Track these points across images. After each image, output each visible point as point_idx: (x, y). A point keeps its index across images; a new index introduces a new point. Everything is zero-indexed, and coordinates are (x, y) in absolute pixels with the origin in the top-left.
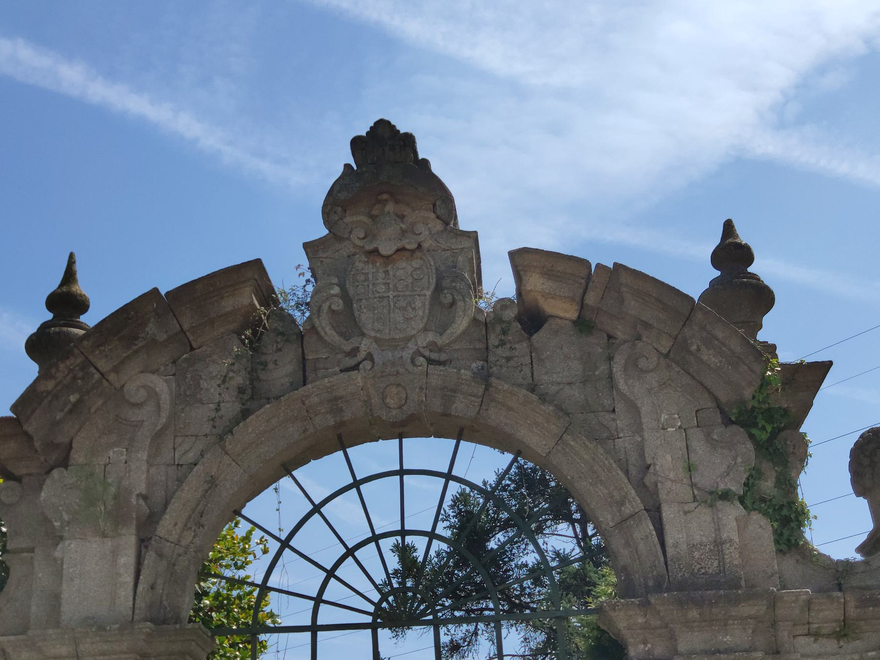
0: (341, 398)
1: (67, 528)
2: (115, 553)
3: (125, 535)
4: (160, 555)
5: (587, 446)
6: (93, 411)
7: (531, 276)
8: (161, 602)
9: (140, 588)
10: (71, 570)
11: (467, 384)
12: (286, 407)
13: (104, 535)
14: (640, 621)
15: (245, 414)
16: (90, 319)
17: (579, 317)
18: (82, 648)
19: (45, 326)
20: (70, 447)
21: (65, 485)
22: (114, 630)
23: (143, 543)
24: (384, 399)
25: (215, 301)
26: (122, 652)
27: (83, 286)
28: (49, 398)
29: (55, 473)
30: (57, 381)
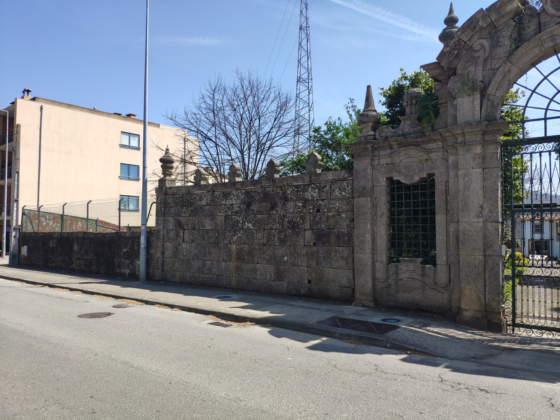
0: (556, 35)
4: (489, 100)
9: (482, 111)
13: (469, 96)
15: (517, 48)
16: (459, 25)
18: (465, 131)
19: (444, 30)
23: (482, 97)
27: (456, 14)
28: (448, 53)
29: (452, 78)
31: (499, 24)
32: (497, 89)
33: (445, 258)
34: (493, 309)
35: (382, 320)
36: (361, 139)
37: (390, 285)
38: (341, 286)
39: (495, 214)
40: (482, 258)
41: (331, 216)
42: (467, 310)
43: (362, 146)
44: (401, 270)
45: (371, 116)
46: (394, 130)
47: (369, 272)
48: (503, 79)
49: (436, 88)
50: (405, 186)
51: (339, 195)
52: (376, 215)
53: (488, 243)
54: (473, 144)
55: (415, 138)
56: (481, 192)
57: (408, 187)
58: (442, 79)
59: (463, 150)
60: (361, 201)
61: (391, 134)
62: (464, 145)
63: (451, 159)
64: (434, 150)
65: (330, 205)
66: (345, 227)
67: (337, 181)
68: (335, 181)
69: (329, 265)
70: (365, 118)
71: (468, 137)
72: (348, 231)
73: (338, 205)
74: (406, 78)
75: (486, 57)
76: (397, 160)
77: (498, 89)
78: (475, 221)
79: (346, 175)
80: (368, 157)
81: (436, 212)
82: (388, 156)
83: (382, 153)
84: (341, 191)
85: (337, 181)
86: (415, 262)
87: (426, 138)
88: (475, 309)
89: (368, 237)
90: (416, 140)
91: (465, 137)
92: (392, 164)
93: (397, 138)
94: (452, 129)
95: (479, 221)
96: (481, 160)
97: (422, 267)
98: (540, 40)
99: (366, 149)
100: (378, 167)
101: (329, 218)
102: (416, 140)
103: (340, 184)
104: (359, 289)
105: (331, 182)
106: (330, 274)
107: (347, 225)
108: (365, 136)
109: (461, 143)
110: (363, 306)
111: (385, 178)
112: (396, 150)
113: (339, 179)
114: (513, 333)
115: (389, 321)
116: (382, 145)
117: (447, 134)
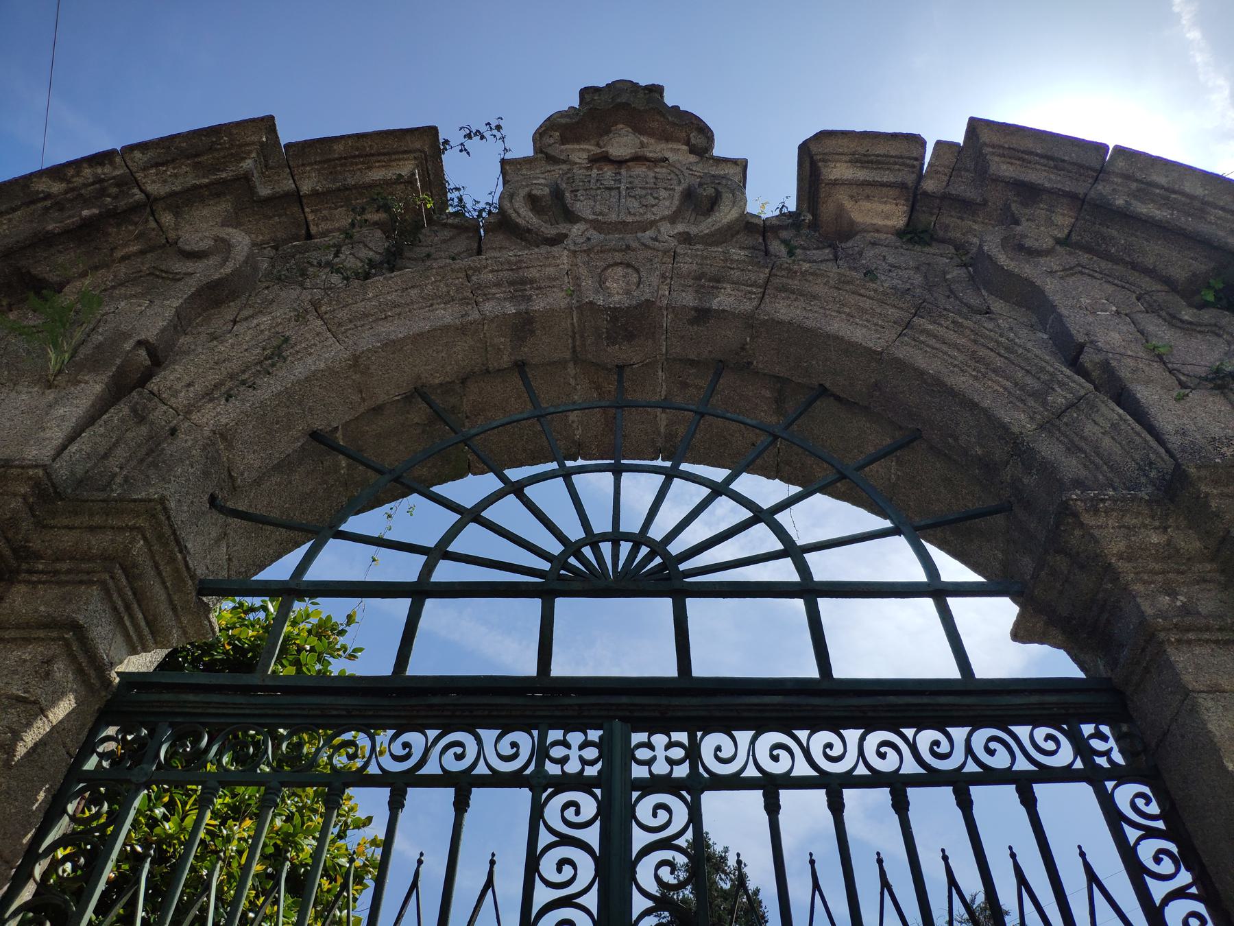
0: (532, 281)
4: (140, 417)
5: (961, 325)
6: (118, 254)
7: (835, 167)
9: (73, 448)
11: (739, 268)
12: (439, 278)
14: (1155, 539)
17: (908, 224)
24: (602, 282)
25: (359, 169)
28: (48, 203)
30: (71, 185)
31: (324, 226)
98: (468, 278)
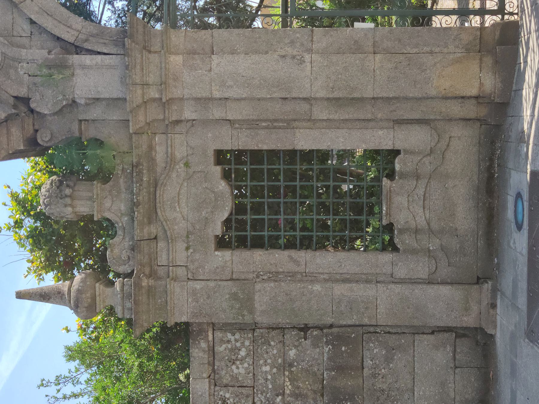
1: (67, 96)
2: (83, 67)
3: (73, 61)
4: (86, 40)
8: (114, 40)
9: (105, 51)
10: (93, 93)
13: (73, 75)
18: (138, 81)
20: (16, 98)
21: (41, 99)
22: (129, 60)
23: (78, 50)
26: (142, 58)
29: (33, 105)
32: (69, 27)
33: (380, 132)
34: (475, 39)
35: (519, 227)
36: (128, 309)
37: (443, 248)
38: (452, 365)
39: (298, 35)
40: (378, 57)
41: (293, 387)
42: (481, 84)
43: (144, 298)
44: (407, 222)
45: (81, 284)
46: (120, 232)
47: (418, 290)
48: (51, 16)
49: (47, 139)
50: (236, 214)
51: (246, 365)
52: (296, 273)
53: (351, 48)
54: (166, 68)
55: (141, 185)
56: (256, 58)
57: (239, 209)
58: (31, 128)
59: (175, 87)
60: (261, 306)
61: (127, 239)
62: (165, 83)
63: (189, 114)
64: (169, 149)
65: (267, 387)
66: (318, 350)
67: (214, 371)
68: (213, 374)
69: (406, 396)
70: (84, 296)
71: (151, 79)
72: (327, 343)
73: (268, 368)
74: (18, 224)
75: (6, 42)
76: (181, 227)
77: (69, 25)
78: (309, 68)
79: (203, 345)
80: (168, 287)
81: (291, 148)
82: (170, 245)
83: (163, 260)
84: (237, 359)
85: (214, 371)
86: (390, 191)
87: (145, 164)
88: (479, 69)
89: (340, 289)
90: (145, 185)
91: (151, 83)
92: (187, 237)
93: (136, 222)
94: (133, 102)
95: (309, 60)
96: (196, 56)
97: (400, 178)
99: (150, 290)
100: (191, 267)
101: (297, 392)
102: (145, 185)
103: (220, 361)
104: (456, 317)
105: (215, 385)
106: (428, 393)
107: (315, 345)
108: (123, 298)
109: (161, 92)
110: (493, 306)
111: (216, 253)
112: (159, 229)
113: (209, 363)
114: (517, 14)
115: (520, 217)
116: (147, 257)
117: (141, 118)
